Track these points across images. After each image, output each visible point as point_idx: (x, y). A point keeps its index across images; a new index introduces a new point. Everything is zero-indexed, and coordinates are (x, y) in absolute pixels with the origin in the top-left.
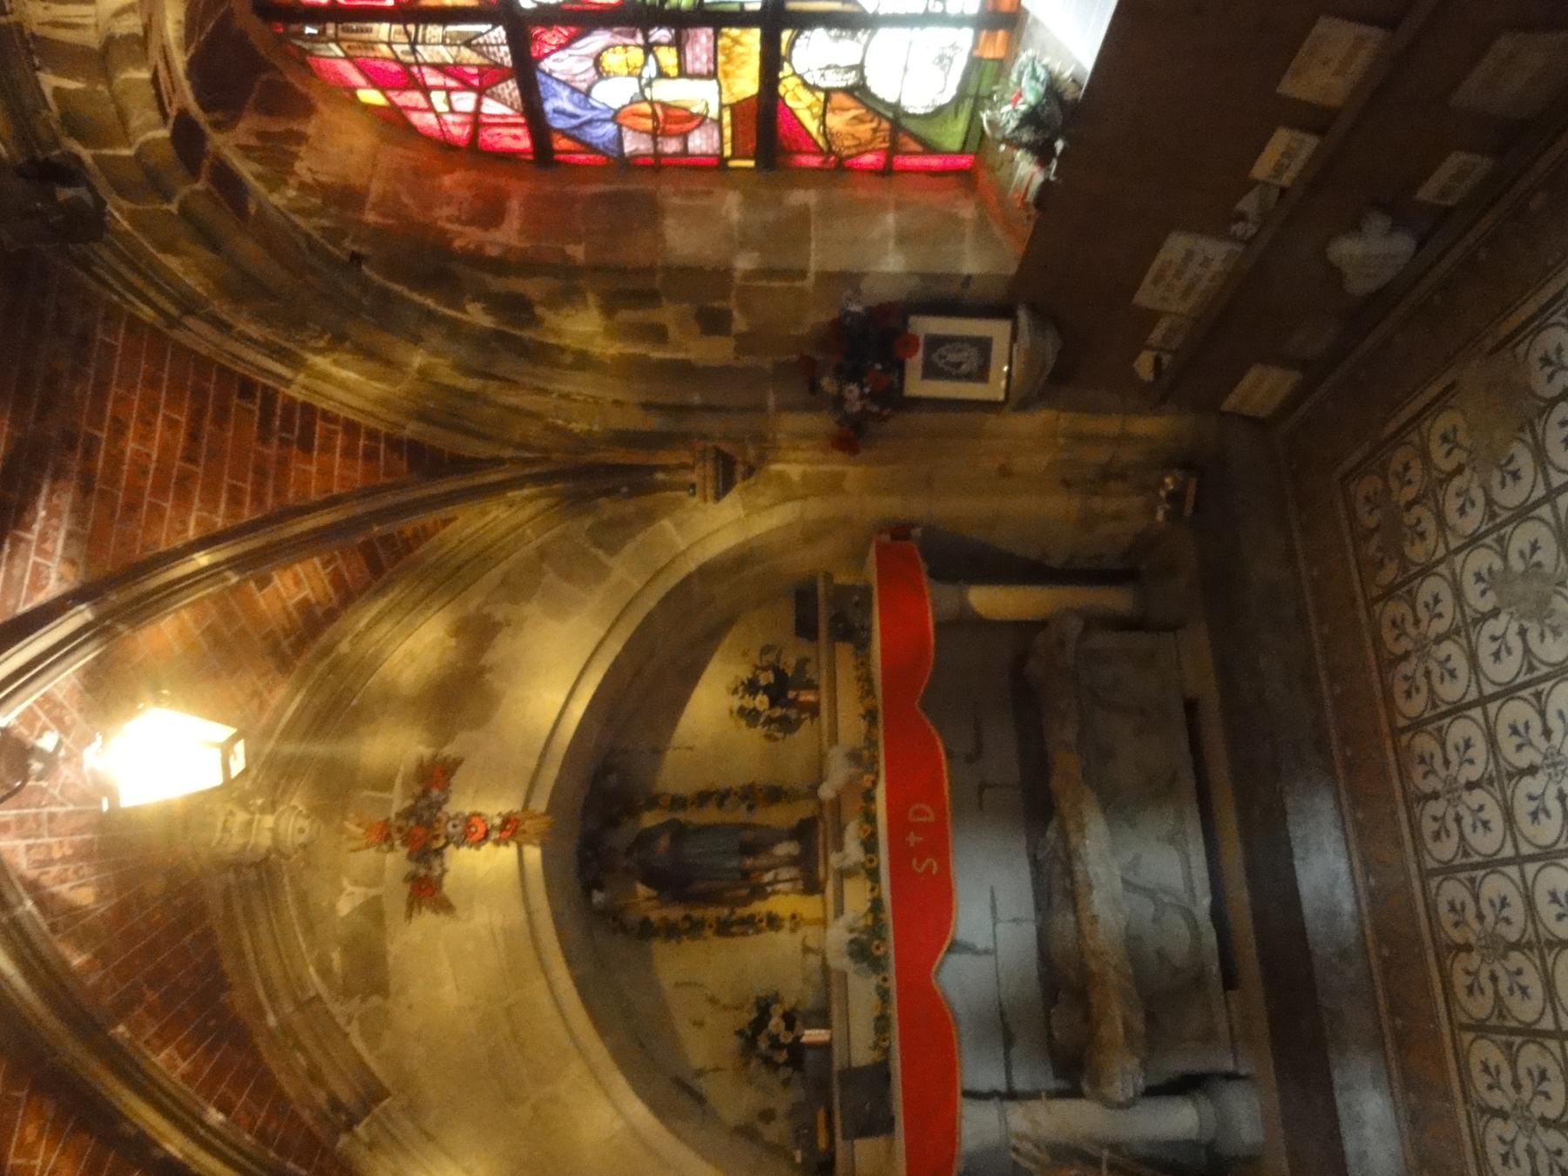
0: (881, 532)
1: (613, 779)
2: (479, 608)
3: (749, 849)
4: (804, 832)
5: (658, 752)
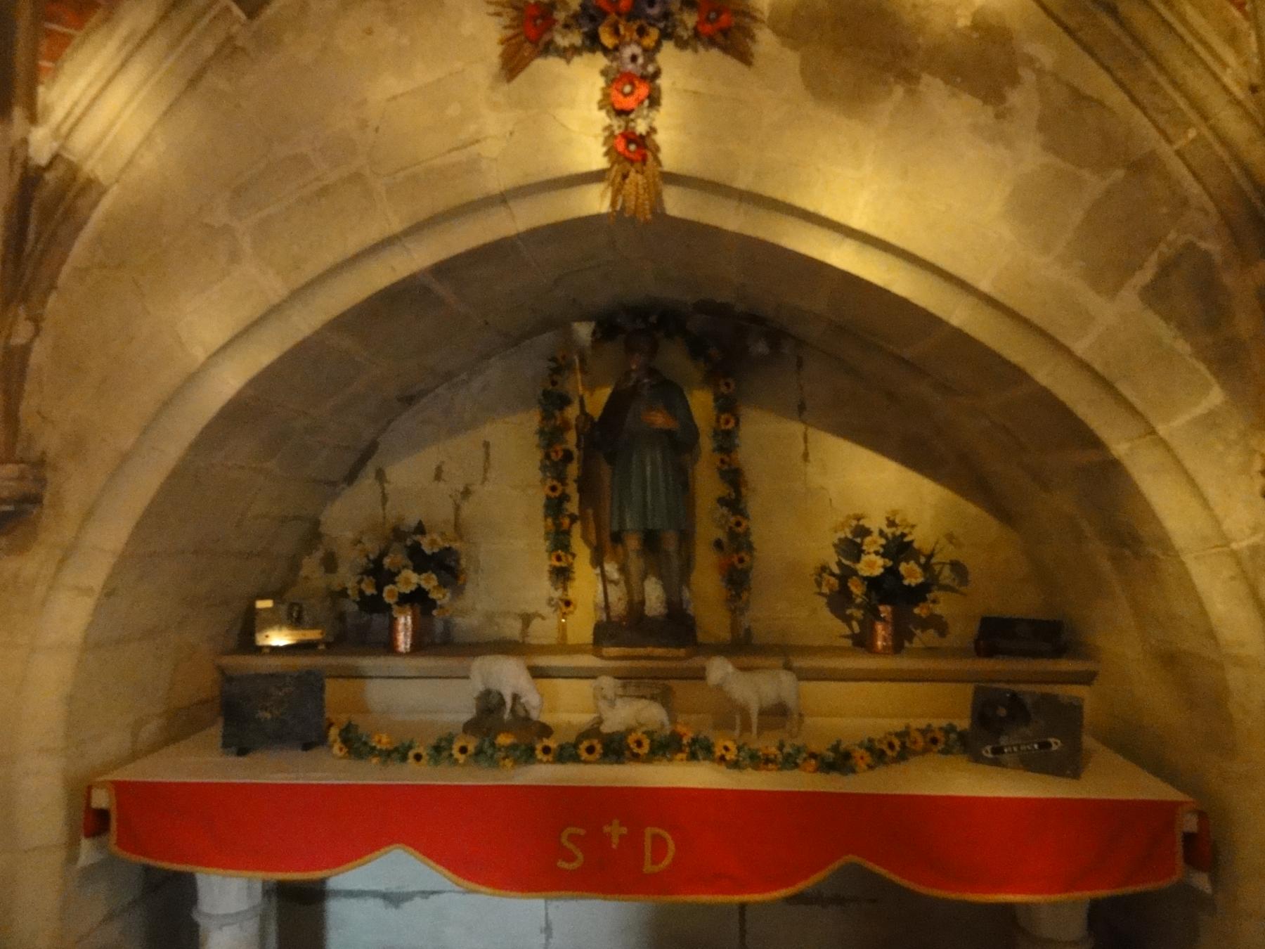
0: (1202, 815)
1: (761, 348)
2: (1031, 61)
3: (651, 542)
4: (677, 627)
5: (800, 411)
